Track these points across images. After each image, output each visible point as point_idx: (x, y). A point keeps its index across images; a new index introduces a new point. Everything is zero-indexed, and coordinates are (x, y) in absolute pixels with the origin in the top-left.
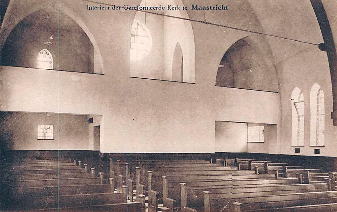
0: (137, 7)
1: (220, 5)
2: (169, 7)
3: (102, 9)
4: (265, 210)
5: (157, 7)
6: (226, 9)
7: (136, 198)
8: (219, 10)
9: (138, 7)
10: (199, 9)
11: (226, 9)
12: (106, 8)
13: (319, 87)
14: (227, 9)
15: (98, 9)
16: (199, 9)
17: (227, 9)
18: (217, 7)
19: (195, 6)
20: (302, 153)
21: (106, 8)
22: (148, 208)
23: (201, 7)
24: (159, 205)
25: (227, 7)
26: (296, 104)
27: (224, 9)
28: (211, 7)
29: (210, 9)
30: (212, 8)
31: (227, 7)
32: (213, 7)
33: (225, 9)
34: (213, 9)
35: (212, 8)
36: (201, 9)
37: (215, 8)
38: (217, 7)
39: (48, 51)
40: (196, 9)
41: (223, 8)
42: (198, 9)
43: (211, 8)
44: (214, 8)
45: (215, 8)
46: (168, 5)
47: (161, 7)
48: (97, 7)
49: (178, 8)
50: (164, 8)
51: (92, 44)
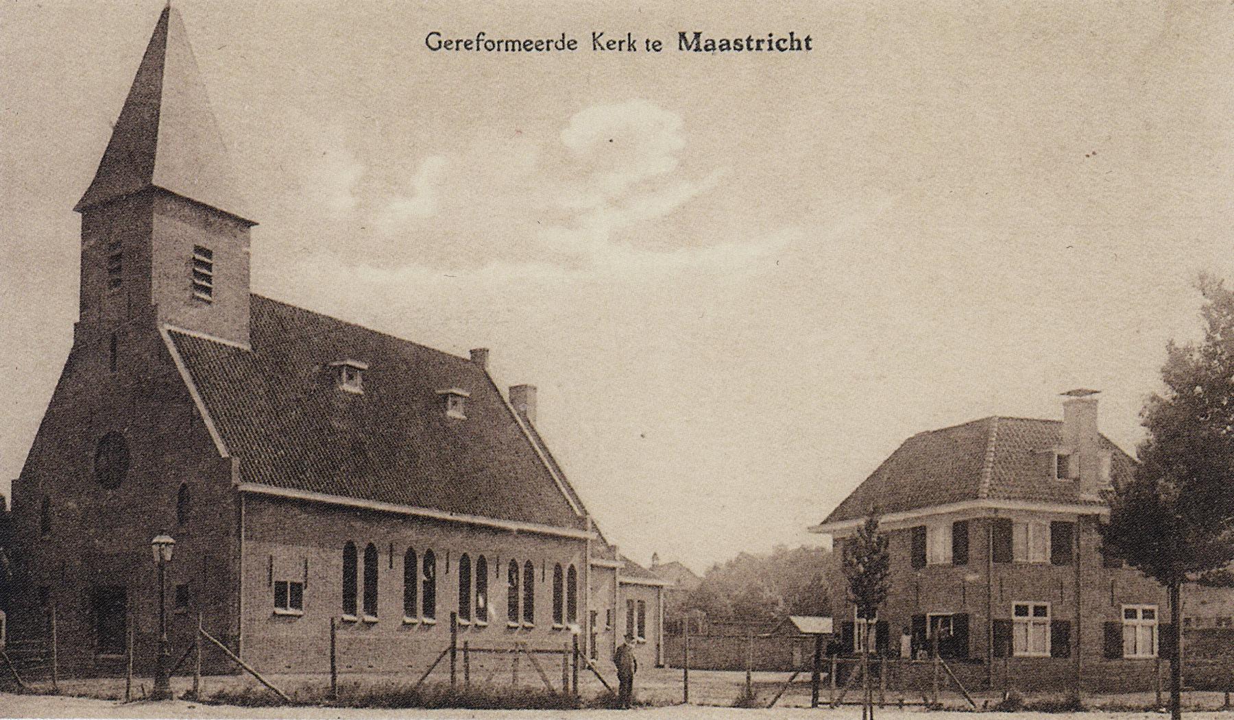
0: (474, 39)
1: (780, 33)
4: (427, 573)
9: (478, 41)
10: (706, 49)
14: (808, 48)
15: (548, 49)
18: (770, 42)
19: (690, 37)
22: (246, 347)
23: (728, 43)
25: (808, 39)
27: (796, 46)
28: (749, 40)
30: (753, 45)
32: (758, 41)
34: (758, 48)
35: (753, 45)
36: (729, 48)
37: (765, 46)
38: (770, 42)
39: (1137, 696)
41: (796, 44)
42: (702, 47)
44: (762, 46)
49: (630, 45)
51: (1046, 422)
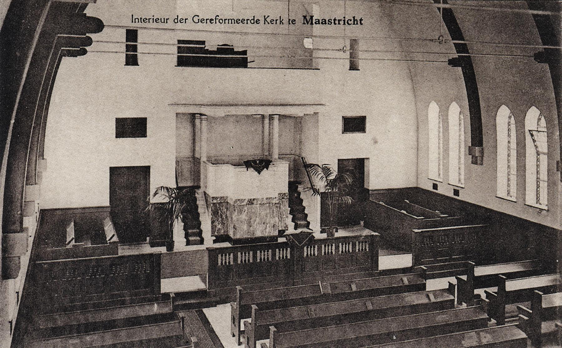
0: (214, 18)
2: (265, 19)
3: (348, 23)
5: (186, 19)
6: (359, 23)
7: (475, 290)
8: (237, 25)
10: (316, 23)
11: (359, 23)
12: (163, 21)
13: (538, 112)
14: (361, 24)
16: (316, 23)
17: (361, 24)
19: (308, 18)
20: (440, 191)
21: (163, 21)
24: (475, 290)
25: (361, 20)
26: (534, 133)
28: (335, 20)
29: (333, 23)
30: (337, 22)
31: (361, 20)
33: (357, 24)
34: (339, 24)
35: (337, 22)
36: (319, 23)
37: (342, 22)
38: (344, 21)
40: (310, 23)
42: (314, 23)
43: (334, 22)
45: (342, 22)
46: (265, 16)
47: (254, 20)
48: (205, 19)
49: (281, 22)
50: (295, 20)
